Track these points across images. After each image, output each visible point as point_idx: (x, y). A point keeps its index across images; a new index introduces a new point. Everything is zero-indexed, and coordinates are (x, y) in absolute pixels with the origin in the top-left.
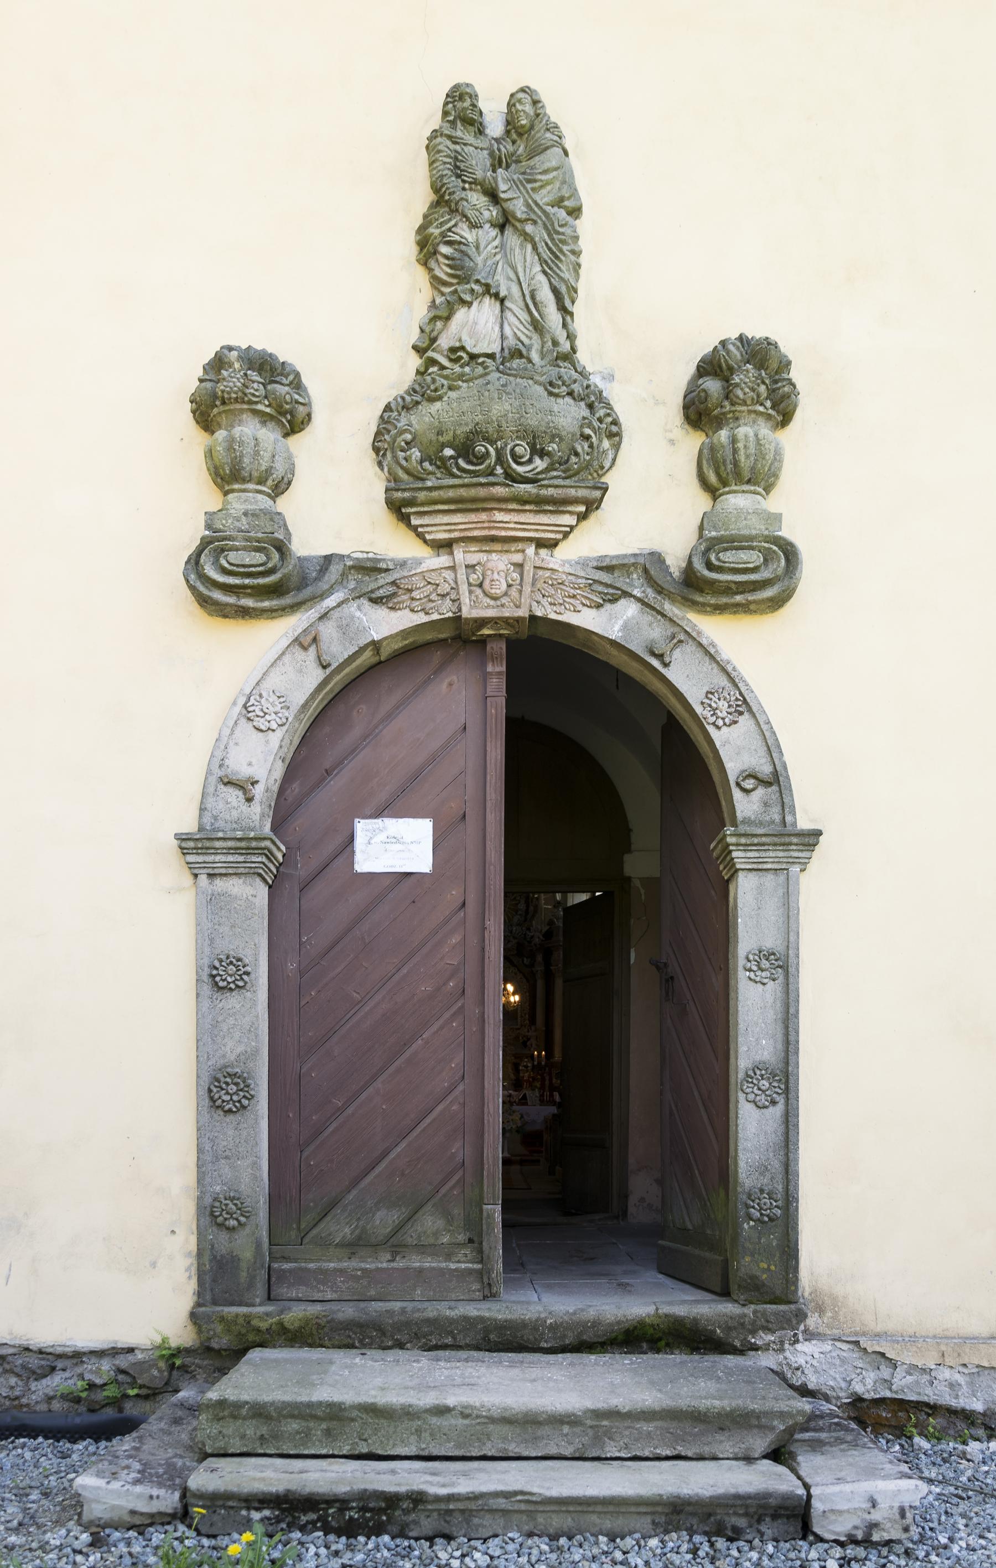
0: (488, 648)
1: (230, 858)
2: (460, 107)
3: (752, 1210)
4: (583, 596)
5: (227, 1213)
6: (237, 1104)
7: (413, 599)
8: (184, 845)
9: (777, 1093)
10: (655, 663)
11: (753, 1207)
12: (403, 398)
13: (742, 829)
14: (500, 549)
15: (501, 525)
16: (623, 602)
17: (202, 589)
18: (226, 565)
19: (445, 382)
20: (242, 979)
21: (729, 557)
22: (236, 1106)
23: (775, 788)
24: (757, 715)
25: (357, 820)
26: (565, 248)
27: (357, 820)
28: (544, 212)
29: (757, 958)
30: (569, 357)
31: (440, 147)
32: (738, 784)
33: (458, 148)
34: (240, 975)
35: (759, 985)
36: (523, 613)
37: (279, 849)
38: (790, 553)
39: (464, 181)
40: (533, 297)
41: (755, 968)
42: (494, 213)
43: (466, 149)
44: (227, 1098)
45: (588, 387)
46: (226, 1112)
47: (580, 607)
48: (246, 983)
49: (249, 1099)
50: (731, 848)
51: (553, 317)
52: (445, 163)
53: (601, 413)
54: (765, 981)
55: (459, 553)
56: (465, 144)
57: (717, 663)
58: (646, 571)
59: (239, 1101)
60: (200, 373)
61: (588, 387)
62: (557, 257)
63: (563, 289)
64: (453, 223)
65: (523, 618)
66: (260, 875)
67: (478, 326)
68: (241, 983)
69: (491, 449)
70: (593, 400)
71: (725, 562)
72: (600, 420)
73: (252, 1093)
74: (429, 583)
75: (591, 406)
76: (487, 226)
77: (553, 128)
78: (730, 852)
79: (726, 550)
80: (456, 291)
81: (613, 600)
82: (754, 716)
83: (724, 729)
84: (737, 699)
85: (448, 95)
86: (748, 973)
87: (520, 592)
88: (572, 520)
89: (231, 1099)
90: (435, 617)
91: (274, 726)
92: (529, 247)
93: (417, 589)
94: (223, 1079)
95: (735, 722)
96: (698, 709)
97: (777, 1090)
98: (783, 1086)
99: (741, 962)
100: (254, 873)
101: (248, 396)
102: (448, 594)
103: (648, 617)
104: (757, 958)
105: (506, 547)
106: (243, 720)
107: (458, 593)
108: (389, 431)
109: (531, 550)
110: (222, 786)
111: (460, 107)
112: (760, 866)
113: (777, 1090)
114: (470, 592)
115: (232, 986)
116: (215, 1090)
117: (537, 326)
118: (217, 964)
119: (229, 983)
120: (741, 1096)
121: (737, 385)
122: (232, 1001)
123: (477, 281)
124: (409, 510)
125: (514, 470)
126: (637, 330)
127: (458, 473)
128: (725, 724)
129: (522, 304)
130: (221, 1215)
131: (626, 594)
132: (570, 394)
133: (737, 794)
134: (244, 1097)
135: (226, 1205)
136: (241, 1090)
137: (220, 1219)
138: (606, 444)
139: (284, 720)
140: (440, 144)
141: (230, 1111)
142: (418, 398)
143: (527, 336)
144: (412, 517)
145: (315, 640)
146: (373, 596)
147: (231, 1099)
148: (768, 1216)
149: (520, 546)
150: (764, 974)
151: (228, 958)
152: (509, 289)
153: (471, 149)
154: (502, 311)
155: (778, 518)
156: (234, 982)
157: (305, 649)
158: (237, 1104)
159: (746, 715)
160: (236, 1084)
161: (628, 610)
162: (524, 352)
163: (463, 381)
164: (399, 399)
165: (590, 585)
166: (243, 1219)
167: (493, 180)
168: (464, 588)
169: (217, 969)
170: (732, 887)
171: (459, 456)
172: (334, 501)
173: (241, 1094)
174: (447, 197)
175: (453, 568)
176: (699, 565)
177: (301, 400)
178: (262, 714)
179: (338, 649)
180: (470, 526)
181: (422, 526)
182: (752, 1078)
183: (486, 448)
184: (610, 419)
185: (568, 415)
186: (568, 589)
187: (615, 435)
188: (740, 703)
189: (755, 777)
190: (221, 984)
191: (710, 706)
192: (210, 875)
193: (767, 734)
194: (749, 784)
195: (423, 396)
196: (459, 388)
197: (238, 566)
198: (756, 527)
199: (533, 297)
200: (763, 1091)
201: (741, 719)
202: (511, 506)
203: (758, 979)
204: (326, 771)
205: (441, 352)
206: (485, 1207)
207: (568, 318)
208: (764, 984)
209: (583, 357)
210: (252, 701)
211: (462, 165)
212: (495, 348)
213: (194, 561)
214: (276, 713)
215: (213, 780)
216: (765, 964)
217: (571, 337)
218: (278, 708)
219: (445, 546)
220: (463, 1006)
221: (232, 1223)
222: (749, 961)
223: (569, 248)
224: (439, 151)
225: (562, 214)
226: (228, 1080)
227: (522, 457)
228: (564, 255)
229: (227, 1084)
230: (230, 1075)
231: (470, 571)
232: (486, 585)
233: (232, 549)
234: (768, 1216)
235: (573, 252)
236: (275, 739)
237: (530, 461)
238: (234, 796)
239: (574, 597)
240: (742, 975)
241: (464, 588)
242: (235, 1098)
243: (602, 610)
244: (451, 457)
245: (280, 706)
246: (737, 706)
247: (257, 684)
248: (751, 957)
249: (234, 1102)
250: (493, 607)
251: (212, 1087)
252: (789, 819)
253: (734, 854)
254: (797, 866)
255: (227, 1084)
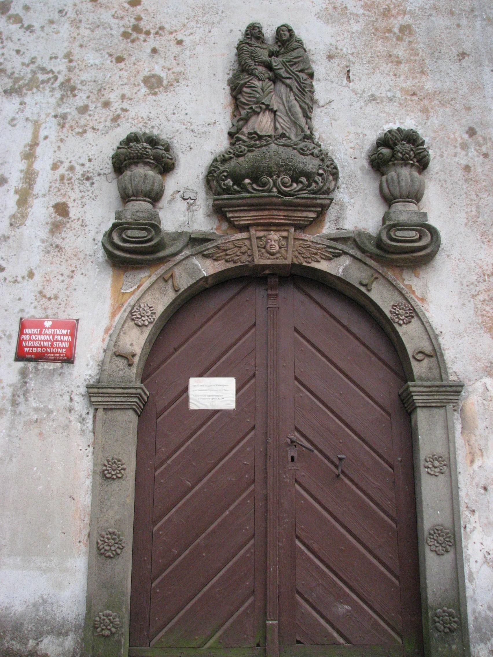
0: (269, 280)
1: (118, 399)
2: (254, 33)
3: (438, 624)
4: (321, 254)
5: (104, 625)
6: (114, 552)
7: (227, 255)
8: (93, 399)
9: (450, 546)
10: (363, 289)
11: (439, 622)
12: (223, 156)
13: (418, 383)
14: (275, 229)
15: (276, 217)
16: (343, 257)
17: (110, 248)
18: (126, 238)
19: (246, 148)
20: (120, 473)
21: (400, 234)
22: (113, 554)
23: (434, 359)
24: (422, 318)
25: (193, 406)
26: (306, 89)
27: (193, 406)
28: (296, 75)
29: (431, 459)
30: (310, 137)
31: (244, 48)
32: (414, 357)
33: (253, 48)
34: (120, 470)
35: (433, 476)
36: (288, 262)
37: (145, 393)
38: (433, 232)
39: (255, 62)
40: (290, 111)
41: (431, 466)
42: (271, 75)
43: (256, 48)
44: (107, 548)
45: (321, 151)
46: (107, 557)
47: (319, 259)
48: (123, 475)
49: (121, 549)
50: (413, 394)
51: (302, 121)
52: (246, 54)
53: (329, 163)
54: (437, 474)
55: (252, 231)
56: (256, 47)
57: (397, 289)
58: (355, 241)
59: (115, 551)
60: (118, 144)
61: (321, 151)
62: (302, 94)
63: (306, 107)
64: (250, 78)
65: (289, 265)
66: (134, 410)
67: (263, 123)
68: (120, 475)
69: (270, 180)
70: (323, 157)
71: (398, 236)
72: (328, 166)
73: (123, 545)
74: (236, 246)
75: (322, 160)
76: (267, 80)
77: (299, 41)
78: (412, 396)
79: (398, 230)
80: (251, 108)
81: (338, 256)
82: (420, 318)
83: (404, 326)
84: (410, 309)
85: (247, 28)
86: (426, 469)
87: (287, 251)
88: (313, 215)
89: (110, 549)
90: (239, 264)
91: (146, 323)
92: (288, 89)
93: (229, 249)
94: (106, 536)
95: (410, 322)
96: (389, 315)
97: (449, 543)
98: (452, 541)
99: (422, 463)
100: (130, 409)
101: (143, 158)
102: (246, 252)
103: (357, 265)
104: (431, 459)
105: (279, 228)
106: (130, 320)
107: (252, 252)
108: (215, 172)
109: (292, 230)
110: (115, 357)
111: (254, 33)
112: (428, 405)
113: (449, 543)
114: (259, 251)
115: (114, 477)
116: (100, 543)
117: (295, 123)
118: (106, 463)
119: (113, 475)
120: (427, 549)
121: (399, 151)
122: (115, 485)
123: (263, 103)
124: (226, 209)
125: (281, 189)
126: (345, 125)
127: (252, 191)
128: (404, 323)
129: (285, 114)
130: (100, 626)
131: (345, 253)
132: (312, 154)
133: (414, 363)
134: (118, 547)
135: (104, 620)
136: (117, 543)
137: (102, 551)
138: (331, 178)
139: (152, 320)
140: (244, 46)
141: (109, 557)
142: (232, 155)
143: (288, 128)
144: (227, 213)
145: (172, 276)
146: (205, 253)
147: (110, 549)
148: (449, 628)
149: (286, 228)
150: (436, 470)
151: (112, 459)
152: (278, 107)
153: (259, 49)
154: (275, 117)
155: (425, 215)
156: (115, 474)
157: (166, 281)
158: (114, 552)
159: (416, 318)
160: (114, 539)
161: (346, 261)
162: (287, 135)
163: (256, 148)
164: (222, 156)
165: (325, 248)
166: (113, 630)
167: (269, 65)
168: (255, 248)
169: (105, 466)
170: (413, 417)
171: (253, 183)
172: (183, 209)
173: (117, 545)
174: (247, 68)
175: (249, 239)
176: (384, 238)
177: (170, 157)
178: (139, 317)
179: (184, 282)
180: (259, 217)
181: (232, 217)
182: (433, 535)
183: (268, 179)
184: (333, 166)
185: (311, 164)
186: (313, 250)
187: (335, 175)
188: (411, 311)
189: (423, 353)
190: (108, 476)
191: (395, 313)
192: (104, 409)
193: (428, 328)
194: (420, 357)
195: (234, 154)
196: (253, 151)
197: (132, 237)
198: (415, 219)
199: (290, 111)
200: (441, 544)
201: (413, 320)
202: (282, 208)
203: (432, 473)
204: (175, 348)
205: (244, 135)
206: (267, 622)
207: (309, 120)
208: (436, 476)
209: (316, 134)
210: (135, 309)
211: (254, 55)
212: (271, 132)
213: (109, 235)
214: (148, 316)
215: (110, 353)
216: (436, 463)
217: (310, 129)
218: (149, 314)
219: (245, 228)
220: (254, 490)
221: (107, 633)
222: (427, 462)
223: (309, 89)
224: (244, 49)
225: (305, 77)
226: (109, 536)
227: (286, 183)
228: (306, 93)
229: (108, 539)
230: (110, 533)
231: (258, 240)
232: (268, 246)
233: (128, 229)
234: (449, 628)
235: (310, 91)
236: (147, 331)
237: (291, 185)
238: (121, 363)
239: (316, 254)
240: (423, 471)
241: (255, 248)
242: (113, 548)
243: (332, 261)
244: (249, 184)
245: (150, 312)
246: (410, 313)
247: (138, 300)
248: (428, 460)
249: (112, 551)
250: (272, 259)
251: (99, 541)
252: (444, 376)
253: (415, 397)
254: (451, 404)
255: (108, 539)
